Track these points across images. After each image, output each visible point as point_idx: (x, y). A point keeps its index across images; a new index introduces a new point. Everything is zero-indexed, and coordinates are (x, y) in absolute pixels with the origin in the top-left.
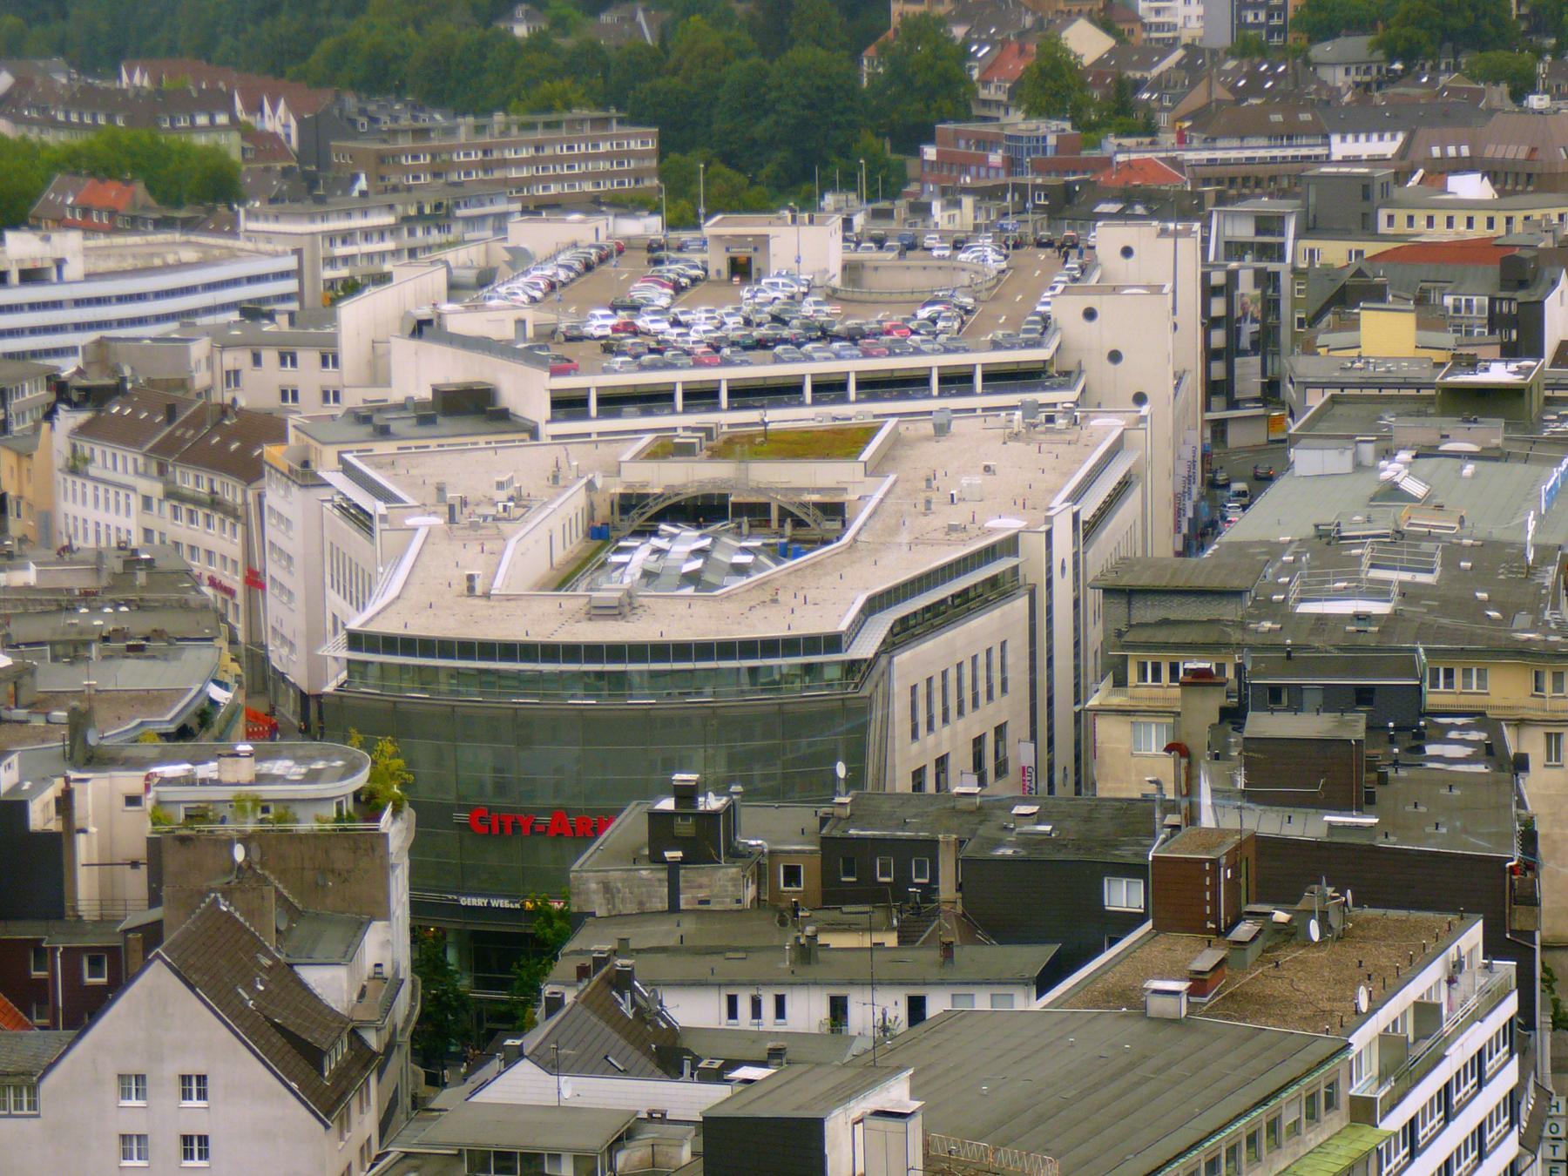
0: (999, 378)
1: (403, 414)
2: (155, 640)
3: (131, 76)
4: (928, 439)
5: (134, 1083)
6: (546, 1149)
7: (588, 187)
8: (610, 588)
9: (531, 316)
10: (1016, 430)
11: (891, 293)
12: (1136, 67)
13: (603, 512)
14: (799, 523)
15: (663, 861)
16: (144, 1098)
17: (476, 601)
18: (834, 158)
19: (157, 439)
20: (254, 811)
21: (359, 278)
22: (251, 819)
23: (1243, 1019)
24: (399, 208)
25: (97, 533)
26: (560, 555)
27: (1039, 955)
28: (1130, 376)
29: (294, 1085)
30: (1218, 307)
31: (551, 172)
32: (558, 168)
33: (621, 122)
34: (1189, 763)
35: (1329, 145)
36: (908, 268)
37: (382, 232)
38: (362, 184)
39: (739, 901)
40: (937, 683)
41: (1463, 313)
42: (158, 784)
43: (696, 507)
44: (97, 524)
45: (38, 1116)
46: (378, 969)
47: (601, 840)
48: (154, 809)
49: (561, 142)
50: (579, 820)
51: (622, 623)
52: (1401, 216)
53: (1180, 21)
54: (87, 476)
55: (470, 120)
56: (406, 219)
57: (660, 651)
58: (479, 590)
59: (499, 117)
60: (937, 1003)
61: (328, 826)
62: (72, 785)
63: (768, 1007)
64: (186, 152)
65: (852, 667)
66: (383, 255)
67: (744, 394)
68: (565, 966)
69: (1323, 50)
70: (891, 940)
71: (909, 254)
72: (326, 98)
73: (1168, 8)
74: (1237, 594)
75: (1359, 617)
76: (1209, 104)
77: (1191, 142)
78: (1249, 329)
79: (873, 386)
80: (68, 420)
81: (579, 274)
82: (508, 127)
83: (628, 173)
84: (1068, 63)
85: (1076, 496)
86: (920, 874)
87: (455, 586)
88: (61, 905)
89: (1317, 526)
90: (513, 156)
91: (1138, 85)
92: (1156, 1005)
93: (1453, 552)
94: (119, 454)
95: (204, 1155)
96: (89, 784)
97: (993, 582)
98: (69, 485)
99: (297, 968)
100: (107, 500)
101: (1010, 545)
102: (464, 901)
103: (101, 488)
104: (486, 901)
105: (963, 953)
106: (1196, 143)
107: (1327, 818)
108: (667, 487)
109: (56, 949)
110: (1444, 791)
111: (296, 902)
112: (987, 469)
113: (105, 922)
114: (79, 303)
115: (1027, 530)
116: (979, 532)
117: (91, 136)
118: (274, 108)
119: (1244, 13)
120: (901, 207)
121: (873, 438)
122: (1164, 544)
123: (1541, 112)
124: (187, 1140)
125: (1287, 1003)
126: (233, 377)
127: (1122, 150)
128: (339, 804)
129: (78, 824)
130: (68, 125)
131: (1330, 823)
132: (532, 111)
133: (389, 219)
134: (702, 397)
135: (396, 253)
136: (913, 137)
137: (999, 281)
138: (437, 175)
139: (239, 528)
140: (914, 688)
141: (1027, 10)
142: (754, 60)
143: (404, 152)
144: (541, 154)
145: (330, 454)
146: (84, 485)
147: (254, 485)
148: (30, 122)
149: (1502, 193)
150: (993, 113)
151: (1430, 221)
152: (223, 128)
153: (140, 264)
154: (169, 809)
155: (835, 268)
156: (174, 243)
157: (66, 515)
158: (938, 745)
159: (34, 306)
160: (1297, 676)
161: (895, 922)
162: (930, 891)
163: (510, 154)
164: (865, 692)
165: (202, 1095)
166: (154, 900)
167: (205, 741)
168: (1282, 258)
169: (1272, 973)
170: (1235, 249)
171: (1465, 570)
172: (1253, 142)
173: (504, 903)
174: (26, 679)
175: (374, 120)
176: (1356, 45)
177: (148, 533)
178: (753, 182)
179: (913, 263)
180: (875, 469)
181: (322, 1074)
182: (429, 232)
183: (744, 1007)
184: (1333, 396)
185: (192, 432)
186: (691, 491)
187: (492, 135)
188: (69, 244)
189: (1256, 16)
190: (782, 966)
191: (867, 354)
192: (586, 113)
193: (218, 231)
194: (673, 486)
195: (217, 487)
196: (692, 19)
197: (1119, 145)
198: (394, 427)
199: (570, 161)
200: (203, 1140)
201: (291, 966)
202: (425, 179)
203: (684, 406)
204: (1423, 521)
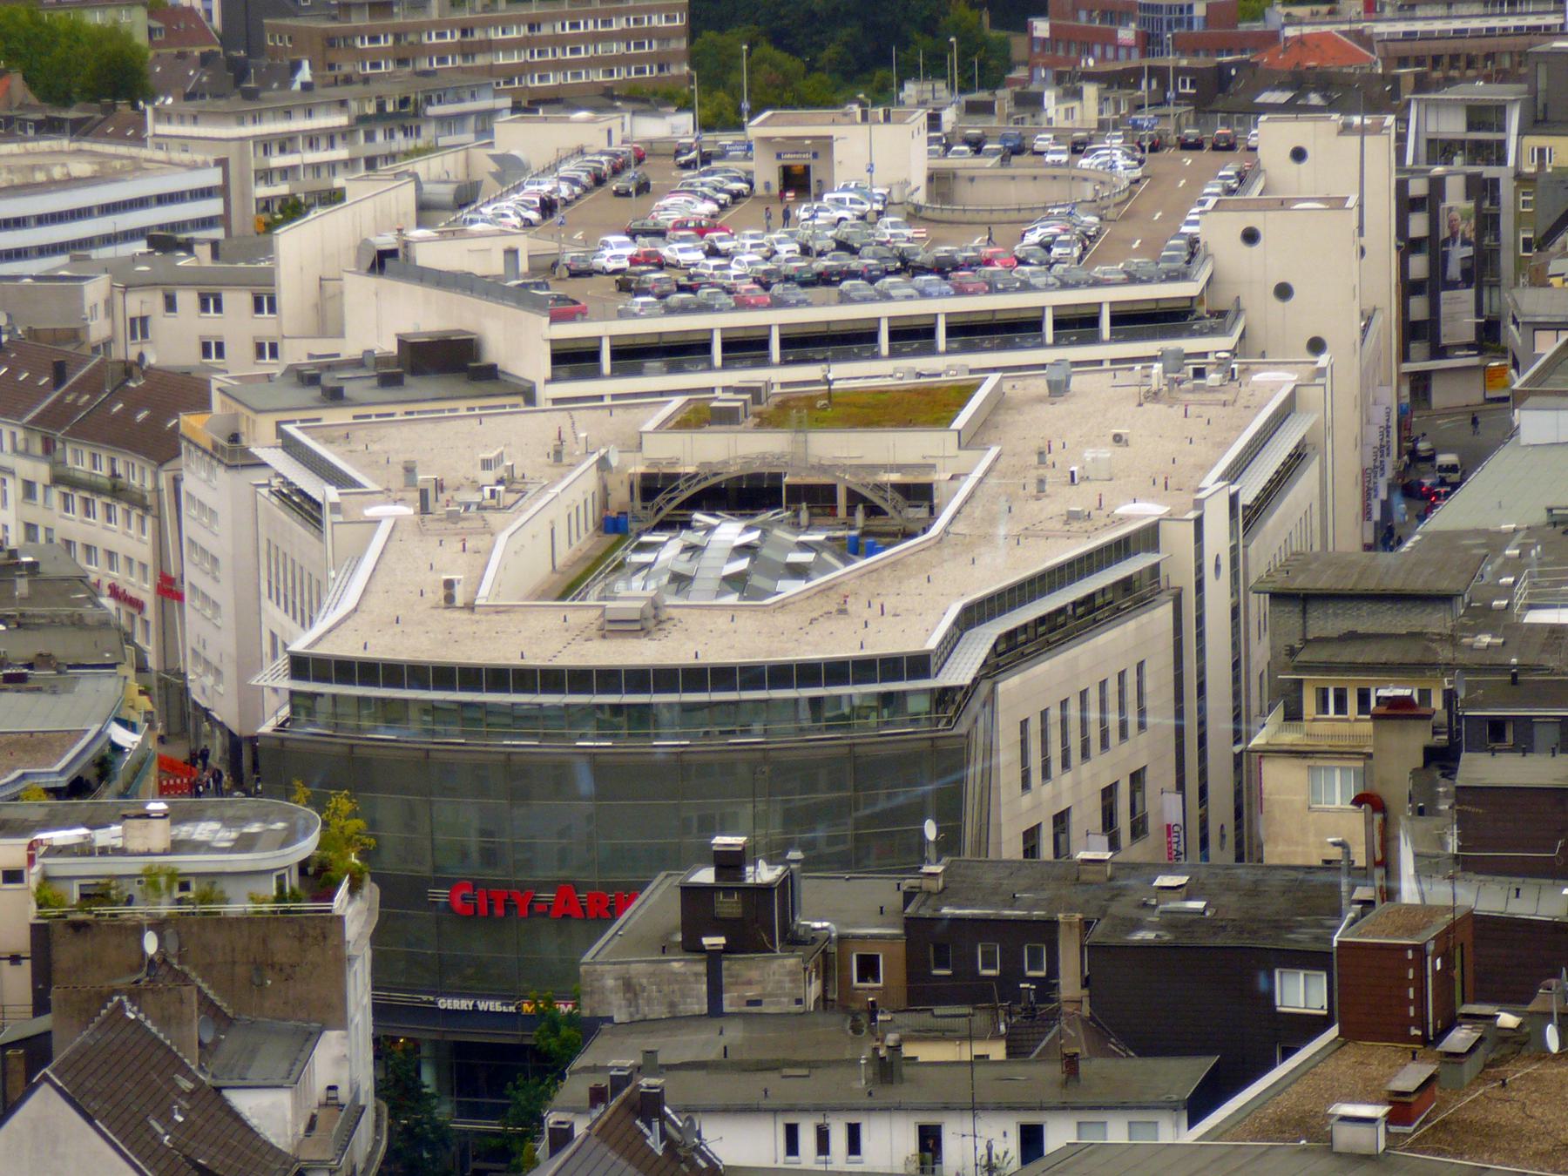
0: (1131, 321)
1: (361, 373)
4: (1040, 400)
7: (599, 77)
8: (632, 593)
9: (525, 245)
13: (620, 496)
14: (873, 511)
15: (701, 949)
17: (457, 614)
20: (169, 888)
21: (302, 197)
22: (165, 899)
23: (1460, 1155)
24: (354, 106)
27: (1189, 1072)
28: (1301, 319)
30: (1418, 225)
32: (559, 52)
34: (1385, 820)
37: (331, 137)
38: (305, 74)
39: (799, 1001)
42: (45, 855)
46: (332, 1094)
49: (561, 17)
51: (645, 641)
56: (362, 119)
57: (695, 677)
60: (1059, 1134)
61: (266, 907)
63: (839, 1139)
64: (75, 33)
66: (332, 166)
67: (802, 344)
68: (575, 1087)
70: (997, 1051)
71: (1015, 159)
74: (1446, 599)
77: (1382, 9)
78: (1459, 254)
79: (969, 332)
81: (587, 190)
83: (649, 58)
85: (1234, 473)
87: (428, 595)
89: (1550, 510)
90: (500, 36)
97: (1126, 585)
101: (1149, 537)
102: (445, 1003)
104: (471, 1004)
108: (702, 464)
115: (1170, 517)
120: (1004, 97)
122: (1349, 533)
125: (1518, 1134)
126: (139, 327)
128: (281, 878)
133: (341, 120)
134: (745, 348)
135: (350, 164)
137: (1132, 194)
138: (402, 62)
139: (149, 522)
143: (359, 32)
144: (469, 39)
145: (265, 426)
153: (17, 179)
154: (59, 887)
155: (919, 179)
158: (1056, 797)
161: (1003, 1028)
162: (1047, 987)
163: (496, 35)
164: (961, 729)
166: (41, 1005)
167: (107, 797)
168: (1502, 160)
169: (1498, 1094)
170: (1441, 149)
172: (1463, 9)
173: (495, 1006)
177: (30, 528)
178: (811, 68)
180: (972, 440)
182: (392, 136)
183: (807, 1139)
186: (734, 470)
187: (473, 10)
191: (960, 291)
193: (119, 137)
195: (120, 468)
197: (1288, 15)
198: (350, 389)
199: (574, 43)
201: (218, 1090)
203: (724, 359)
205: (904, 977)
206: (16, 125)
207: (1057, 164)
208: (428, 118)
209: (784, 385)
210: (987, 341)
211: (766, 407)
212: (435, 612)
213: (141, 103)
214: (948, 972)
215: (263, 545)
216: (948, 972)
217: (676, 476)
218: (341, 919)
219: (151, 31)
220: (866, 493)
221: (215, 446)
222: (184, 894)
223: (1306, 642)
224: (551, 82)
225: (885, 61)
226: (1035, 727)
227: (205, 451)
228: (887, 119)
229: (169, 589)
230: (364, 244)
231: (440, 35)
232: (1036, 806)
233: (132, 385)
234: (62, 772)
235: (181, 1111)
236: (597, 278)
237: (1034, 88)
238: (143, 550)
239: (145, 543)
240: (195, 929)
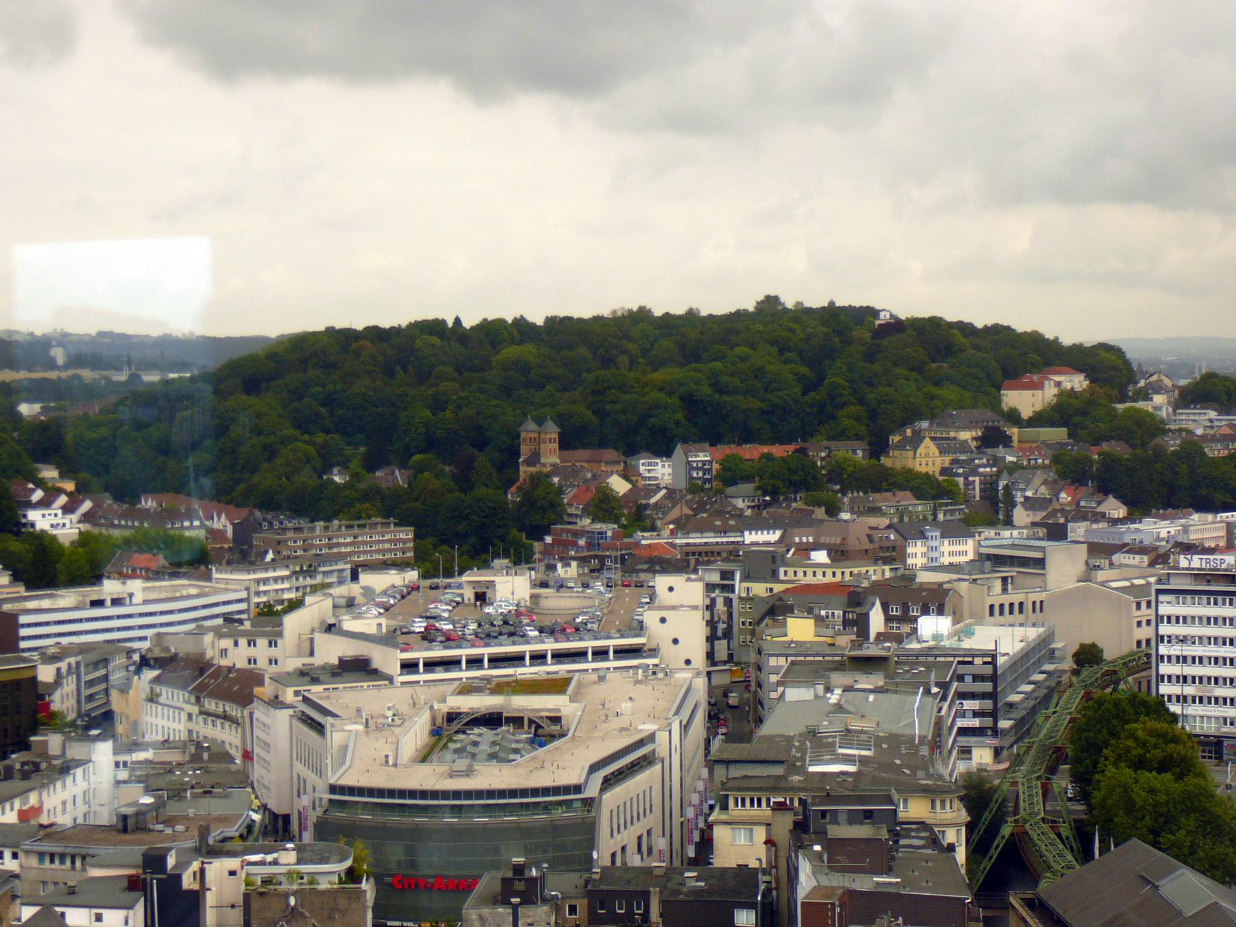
0: (622, 652)
1: (325, 672)
3: (146, 502)
4: (595, 683)
9: (383, 621)
13: (439, 721)
14: (538, 727)
15: (510, 903)
18: (498, 542)
21: (272, 602)
22: (296, 883)
24: (291, 567)
26: (419, 743)
28: (682, 652)
31: (362, 549)
33: (396, 524)
34: (776, 850)
36: (562, 597)
37: (283, 579)
38: (270, 556)
40: (622, 809)
42: (247, 865)
43: (486, 719)
44: (163, 727)
47: (474, 893)
51: (468, 779)
52: (791, 571)
53: (659, 476)
54: (158, 703)
55: (322, 523)
56: (295, 573)
57: (491, 794)
59: (336, 522)
61: (335, 886)
62: (205, 865)
64: (181, 539)
65: (584, 800)
66: (283, 590)
67: (496, 661)
69: (730, 490)
71: (561, 590)
72: (244, 512)
75: (843, 773)
76: (681, 516)
78: (721, 627)
79: (560, 656)
80: (150, 674)
81: (399, 601)
82: (340, 527)
84: (613, 496)
87: (377, 761)
89: (807, 727)
91: (647, 506)
93: (878, 741)
94: (175, 692)
96: (212, 865)
97: (644, 758)
98: (149, 709)
101: (651, 738)
103: (166, 709)
106: (679, 535)
107: (875, 879)
108: (470, 709)
110: (924, 864)
112: (631, 699)
114: (141, 615)
115: (659, 730)
116: (635, 731)
117: (133, 531)
118: (219, 519)
123: (846, 521)
126: (224, 652)
127: (646, 539)
128: (339, 875)
130: (120, 526)
133: (286, 573)
134: (475, 662)
136: (538, 533)
137: (610, 604)
138: (305, 551)
139: (240, 730)
140: (611, 811)
141: (588, 471)
142: (457, 494)
143: (289, 539)
145: (290, 692)
148: (103, 525)
153: (169, 595)
154: (252, 878)
155: (528, 598)
158: (622, 840)
159: (119, 617)
162: (646, 916)
163: (341, 540)
164: (593, 814)
168: (733, 591)
172: (707, 534)
175: (271, 524)
176: (748, 488)
177: (190, 731)
184: (792, 661)
185: (213, 681)
186: (484, 711)
187: (332, 531)
189: (698, 474)
192: (379, 520)
194: (472, 708)
195: (227, 708)
196: (425, 474)
198: (322, 678)
199: (371, 543)
204: (856, 725)
205: (587, 914)
206: (161, 574)
207: (579, 592)
209: (467, 678)
210: (566, 660)
215: (294, 739)
217: (460, 714)
220: (537, 720)
221: (270, 701)
223: (728, 779)
224: (362, 559)
225: (487, 551)
227: (265, 702)
228: (516, 574)
229: (247, 756)
230: (323, 621)
231: (294, 542)
233: (231, 675)
234: (236, 831)
236: (411, 635)
237: (552, 562)
239: (237, 737)
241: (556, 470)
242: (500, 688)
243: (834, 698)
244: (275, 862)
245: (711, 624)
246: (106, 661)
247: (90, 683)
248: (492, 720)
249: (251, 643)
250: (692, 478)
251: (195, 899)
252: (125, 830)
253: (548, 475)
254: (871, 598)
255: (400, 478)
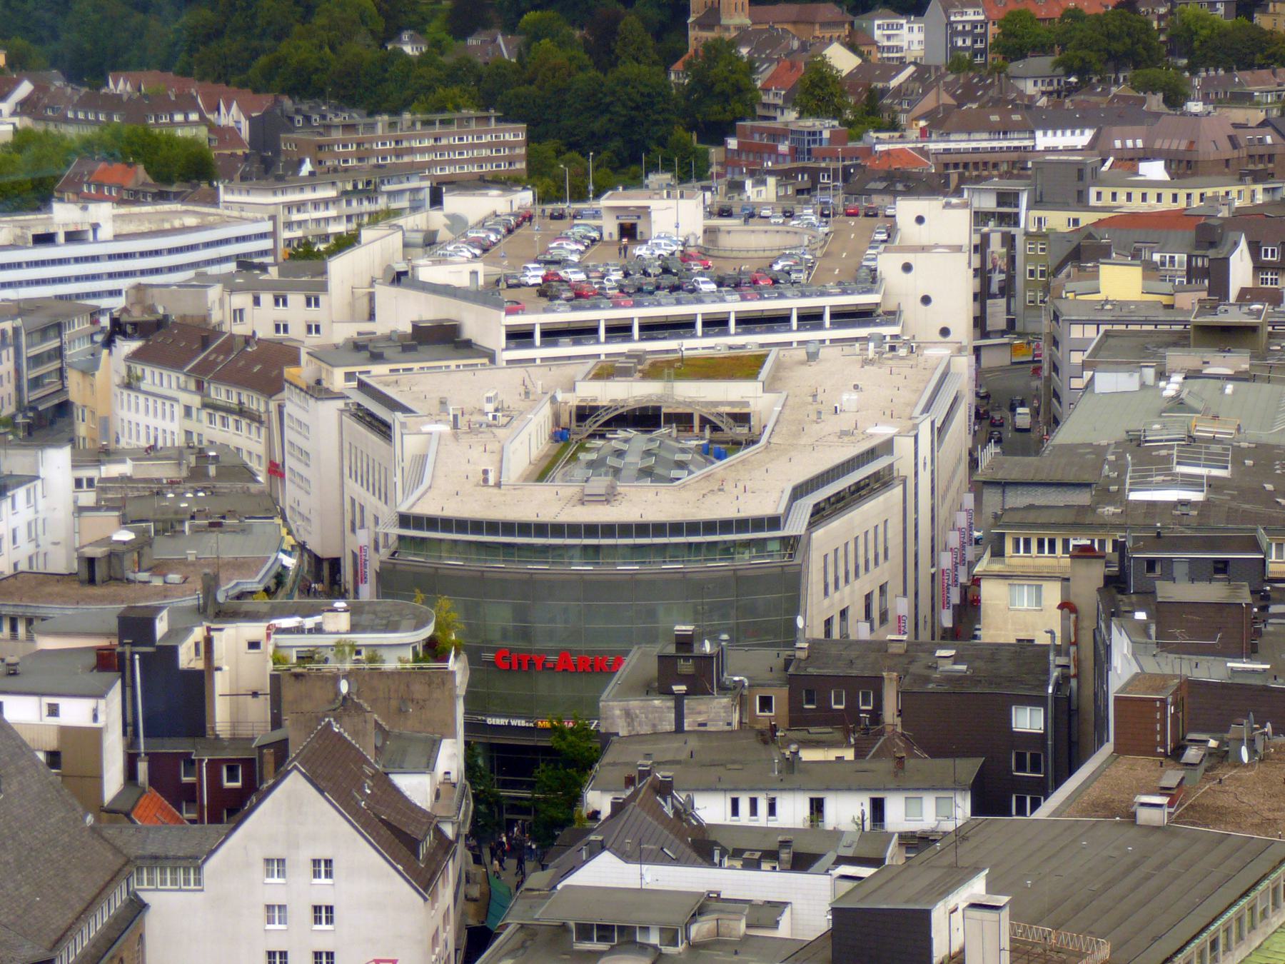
0: (843, 316)
2: (230, 519)
3: (116, 84)
4: (802, 363)
5: (276, 865)
6: (639, 923)
10: (870, 357)
11: (748, 251)
12: (880, 79)
13: (565, 419)
14: (715, 428)
15: (671, 693)
16: (284, 876)
17: (491, 490)
19: (195, 362)
20: (350, 654)
21: (310, 238)
23: (1207, 826)
24: (340, 184)
25: (148, 434)
29: (400, 867)
32: (451, 154)
33: (498, 120)
34: (1077, 617)
35: (1034, 138)
37: (327, 202)
38: (307, 168)
39: (729, 724)
40: (841, 553)
41: (1167, 267)
44: (148, 427)
45: (202, 890)
46: (447, 776)
47: (619, 673)
48: (275, 652)
49: (453, 134)
50: (580, 659)
52: (1107, 192)
54: (139, 390)
55: (386, 117)
56: (345, 193)
58: (492, 481)
60: (898, 815)
61: (408, 666)
62: (212, 633)
63: (763, 806)
64: (171, 141)
65: (785, 541)
66: (327, 220)
67: (652, 329)
70: (849, 755)
72: (266, 100)
73: (897, 35)
74: (1088, 485)
76: (938, 108)
77: (930, 136)
78: (997, 278)
79: (749, 322)
80: (127, 347)
81: (504, 237)
82: (414, 124)
83: (503, 158)
84: (831, 76)
85: (927, 409)
86: (866, 702)
88: (204, 726)
89: (1127, 432)
90: (418, 145)
91: (884, 92)
92: (1144, 816)
93: (1239, 454)
94: (165, 373)
95: (330, 920)
97: (876, 476)
99: (392, 776)
100: (164, 411)
102: (490, 721)
104: (507, 721)
105: (910, 763)
106: (934, 137)
107: (1229, 665)
108: (611, 401)
109: (203, 760)
111: (383, 724)
113: (234, 739)
114: (112, 257)
115: (899, 434)
117: (97, 129)
118: (228, 108)
119: (955, 39)
121: (763, 363)
123: (1196, 115)
124: (317, 909)
126: (239, 314)
127: (883, 143)
128: (414, 648)
129: (216, 664)
130: (76, 121)
131: (1232, 669)
132: (430, 112)
133: (331, 193)
134: (619, 330)
136: (716, 132)
138: (360, 159)
139: (263, 431)
140: (826, 556)
141: (794, 37)
142: (592, 73)
143: (337, 142)
144: (400, 147)
146: (137, 397)
147: (275, 398)
148: (46, 119)
149: (1172, 179)
150: (772, 114)
151: (1129, 196)
152: (194, 124)
153: (154, 227)
154: (284, 652)
155: (700, 233)
156: (176, 212)
157: (122, 420)
158: (842, 600)
159: (78, 260)
160: (1169, 551)
161: (852, 740)
162: (876, 715)
163: (415, 144)
164: (797, 561)
165: (329, 874)
166: (276, 723)
168: (1017, 224)
169: (1218, 788)
171: (1249, 467)
172: (977, 136)
173: (522, 723)
174: (146, 549)
175: (307, 119)
176: (1043, 63)
177: (188, 433)
179: (757, 228)
181: (417, 856)
182: (361, 203)
183: (744, 806)
185: (222, 357)
186: (632, 404)
188: (103, 212)
190: (771, 775)
195: (244, 399)
197: (877, 138)
198: (387, 353)
199: (460, 149)
200: (330, 909)
201: (387, 774)
202: (352, 162)
203: (606, 337)
204: (1204, 429)
206: (141, 195)
208: (383, 193)
210: (758, 327)
211: (645, 366)
212: (478, 488)
213: (215, 183)
214: (813, 707)
215: (346, 446)
216: (813, 707)
218: (453, 673)
219: (210, 140)
220: (712, 418)
221: (308, 387)
222: (359, 657)
223: (1003, 509)
226: (831, 559)
227: (301, 390)
228: (682, 196)
229: (275, 470)
232: (831, 606)
234: (259, 582)
235: (369, 788)
238: (260, 448)
240: (367, 678)
241: (744, 36)
242: (657, 370)
243: (1171, 388)
244: (318, 629)
245: (982, 273)
246: (59, 328)
247: (37, 360)
248: (645, 418)
249: (280, 300)
250: (955, 48)
251: (198, 684)
252: (92, 581)
253: (733, 44)
254: (1232, 236)
255: (505, 48)
